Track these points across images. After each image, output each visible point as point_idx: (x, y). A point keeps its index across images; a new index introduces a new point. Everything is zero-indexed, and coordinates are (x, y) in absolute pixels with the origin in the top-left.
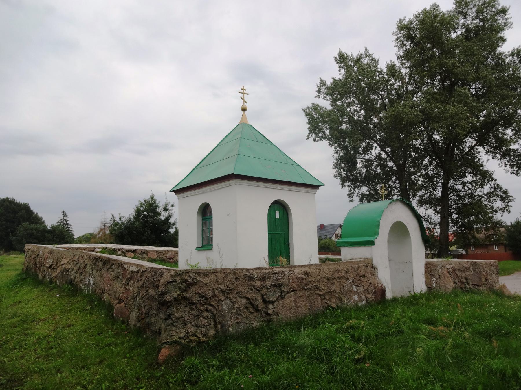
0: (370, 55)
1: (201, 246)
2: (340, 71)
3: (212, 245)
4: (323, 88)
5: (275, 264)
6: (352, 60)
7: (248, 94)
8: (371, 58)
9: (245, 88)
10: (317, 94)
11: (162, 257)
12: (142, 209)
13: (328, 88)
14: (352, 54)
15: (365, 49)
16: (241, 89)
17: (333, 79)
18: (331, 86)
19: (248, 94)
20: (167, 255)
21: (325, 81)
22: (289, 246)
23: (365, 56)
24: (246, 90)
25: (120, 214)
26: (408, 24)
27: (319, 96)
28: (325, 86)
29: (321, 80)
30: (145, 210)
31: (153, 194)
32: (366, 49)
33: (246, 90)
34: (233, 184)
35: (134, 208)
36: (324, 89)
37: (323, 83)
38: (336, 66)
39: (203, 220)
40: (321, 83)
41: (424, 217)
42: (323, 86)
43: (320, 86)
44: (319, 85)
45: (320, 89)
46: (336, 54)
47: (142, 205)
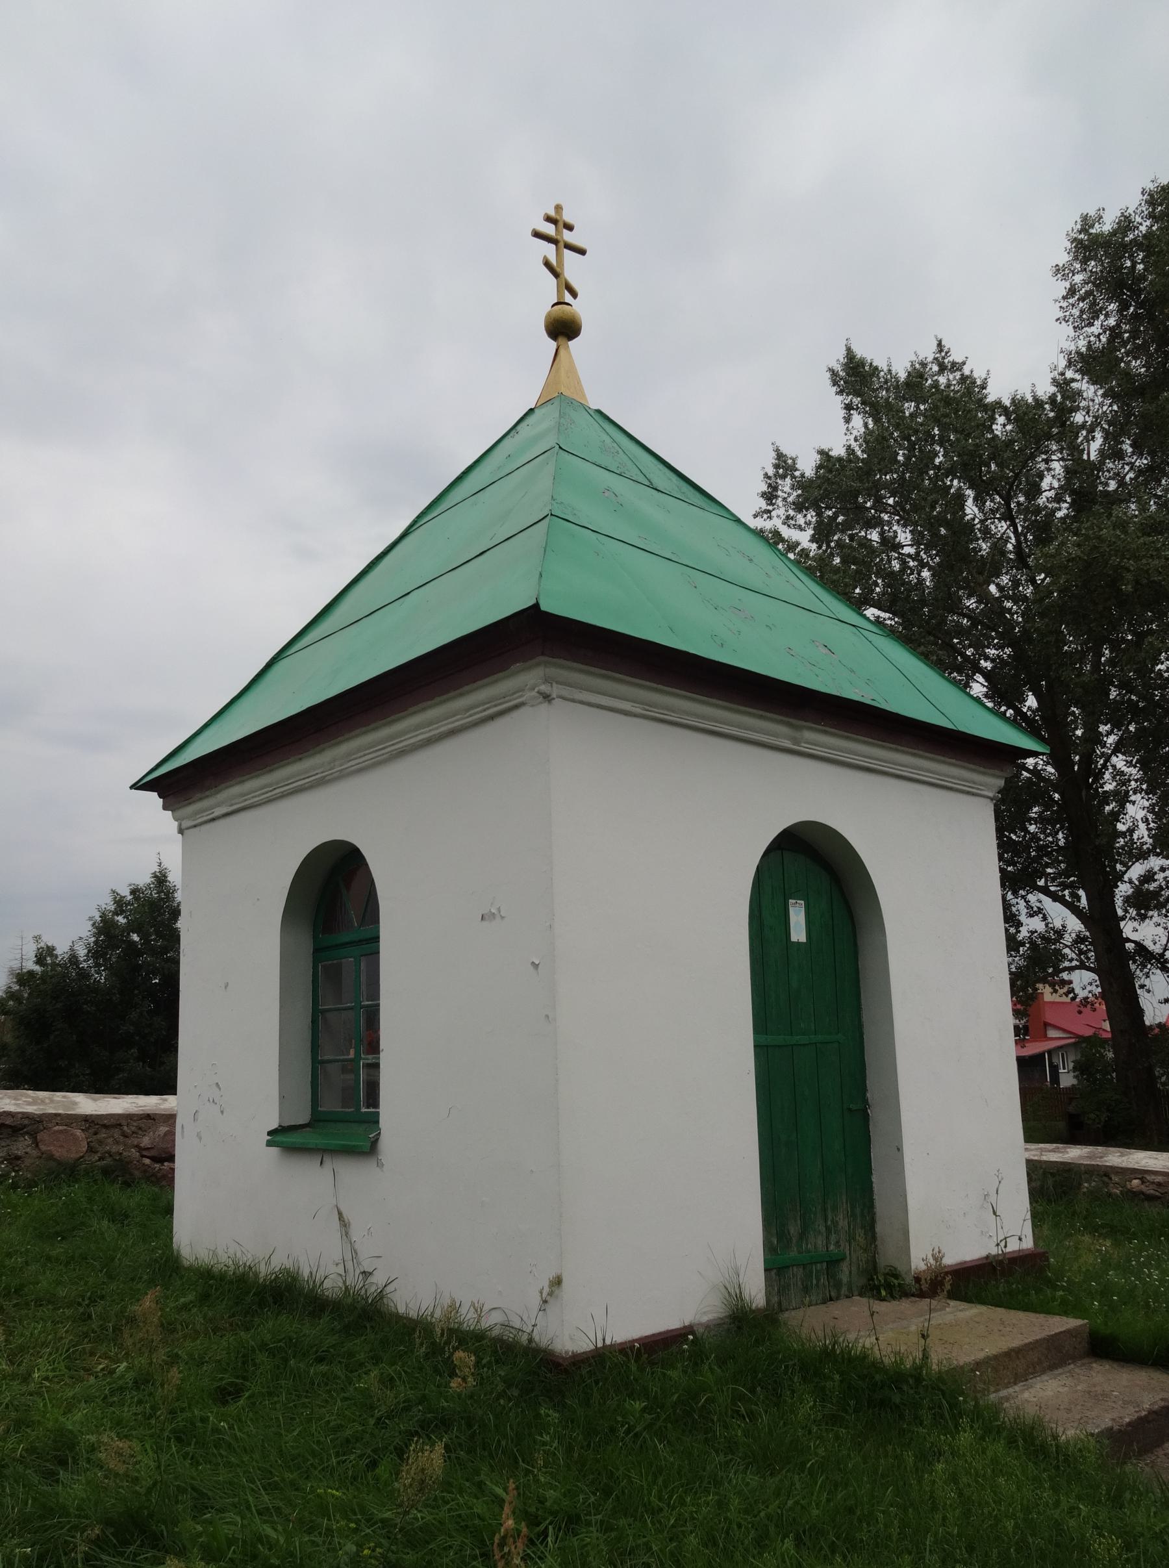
0: (956, 367)
1: (303, 1117)
2: (848, 420)
3: (374, 1120)
4: (786, 485)
5: (793, 1253)
6: (891, 383)
7: (582, 252)
8: (958, 375)
9: (567, 217)
10: (763, 504)
11: (114, 1149)
12: (121, 920)
13: (803, 484)
14: (889, 365)
15: (936, 343)
16: (549, 219)
17: (822, 452)
18: (818, 477)
19: (582, 252)
20: (146, 1141)
21: (794, 460)
22: (866, 1118)
23: (935, 368)
24: (570, 228)
25: (37, 939)
26: (1114, 233)
27: (769, 512)
28: (793, 477)
29: (780, 456)
30: (132, 927)
31: (165, 864)
32: (940, 344)
33: (570, 228)
34: (528, 695)
35: (90, 919)
36: (787, 489)
37: (784, 465)
38: (835, 403)
39: (319, 952)
40: (777, 466)
41: (1162, 955)
42: (783, 477)
43: (776, 475)
44: (771, 471)
45: (775, 489)
46: (836, 359)
47: (120, 902)
